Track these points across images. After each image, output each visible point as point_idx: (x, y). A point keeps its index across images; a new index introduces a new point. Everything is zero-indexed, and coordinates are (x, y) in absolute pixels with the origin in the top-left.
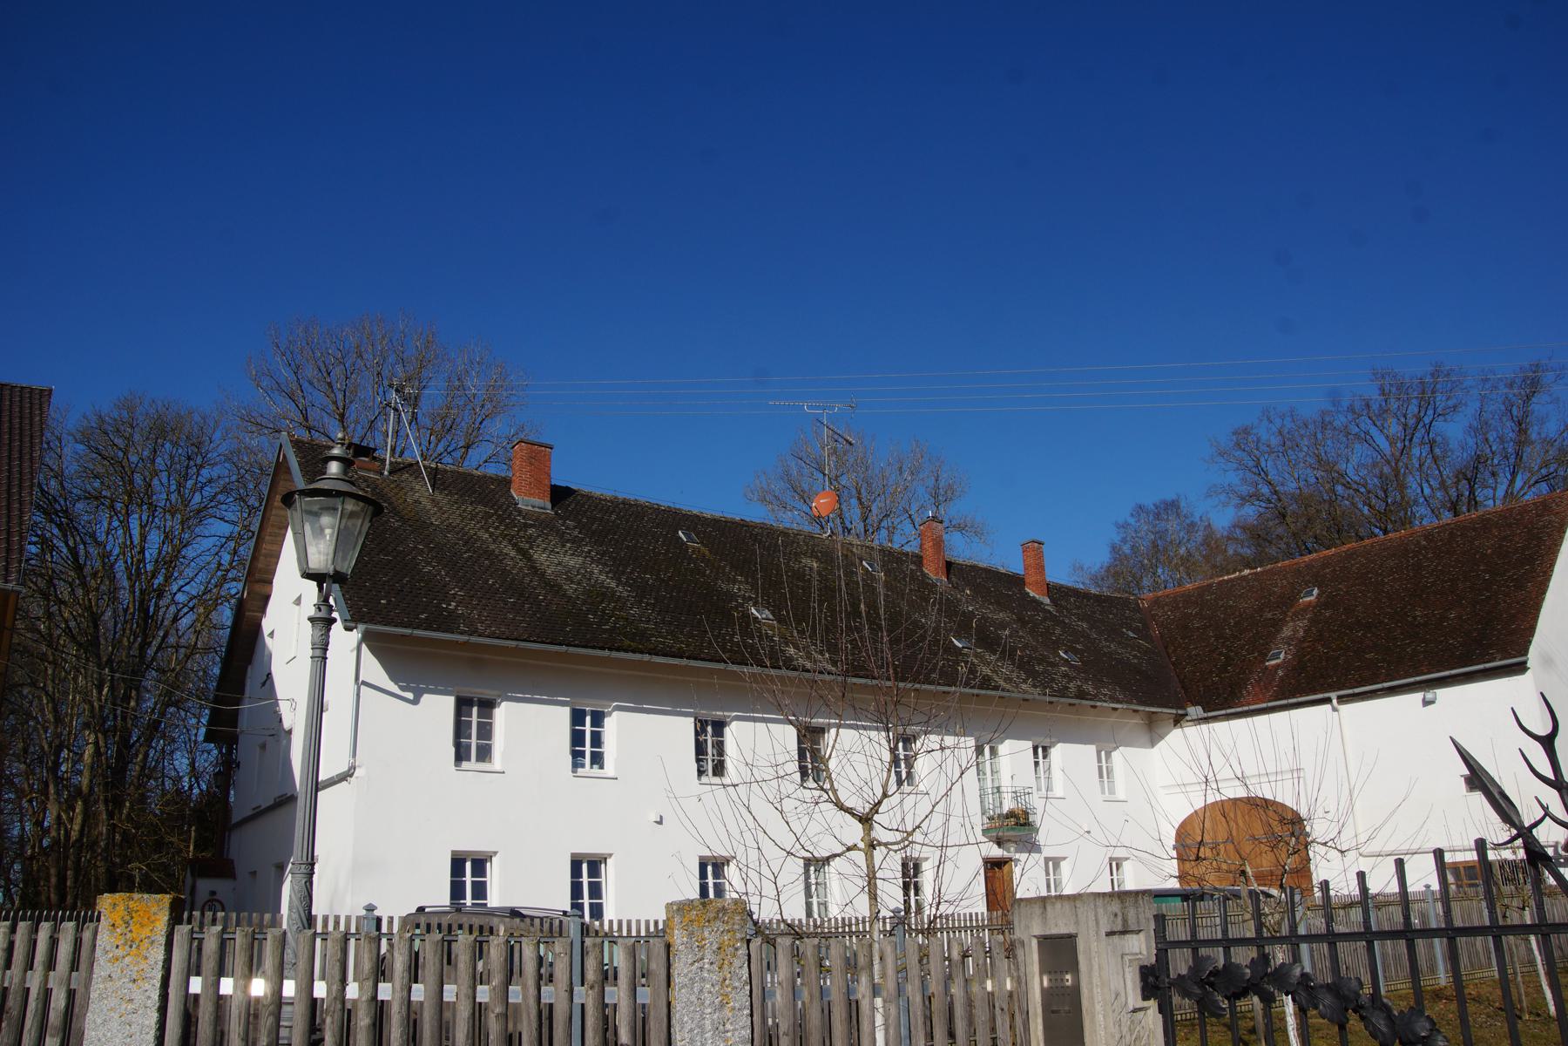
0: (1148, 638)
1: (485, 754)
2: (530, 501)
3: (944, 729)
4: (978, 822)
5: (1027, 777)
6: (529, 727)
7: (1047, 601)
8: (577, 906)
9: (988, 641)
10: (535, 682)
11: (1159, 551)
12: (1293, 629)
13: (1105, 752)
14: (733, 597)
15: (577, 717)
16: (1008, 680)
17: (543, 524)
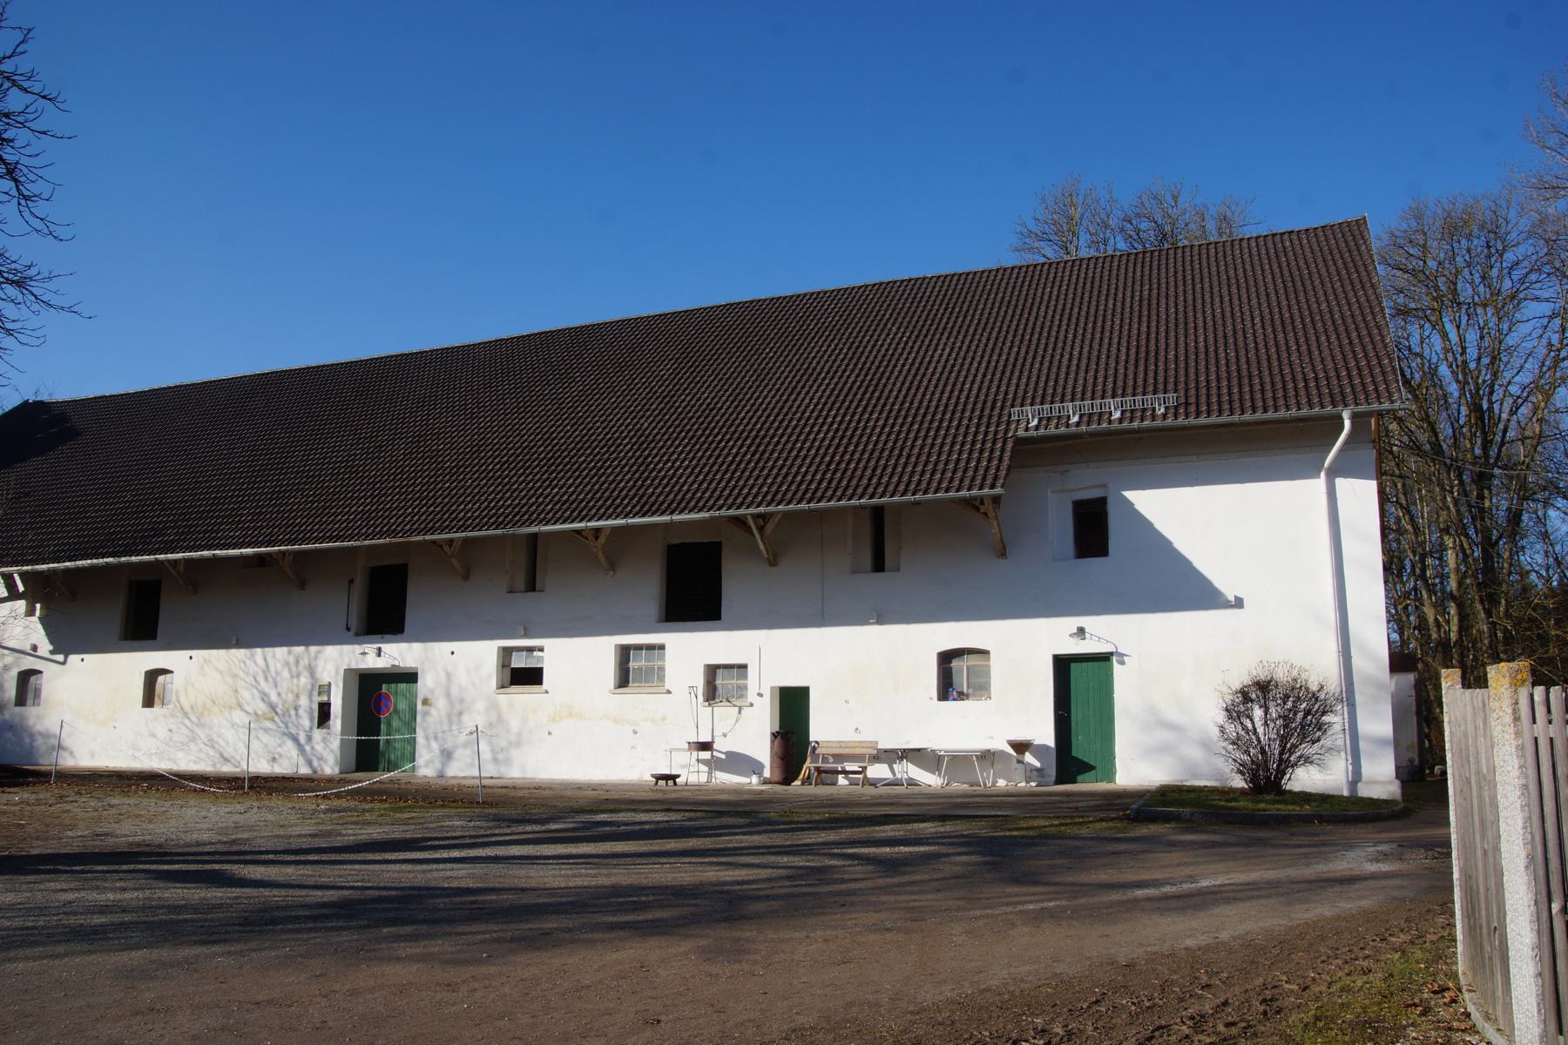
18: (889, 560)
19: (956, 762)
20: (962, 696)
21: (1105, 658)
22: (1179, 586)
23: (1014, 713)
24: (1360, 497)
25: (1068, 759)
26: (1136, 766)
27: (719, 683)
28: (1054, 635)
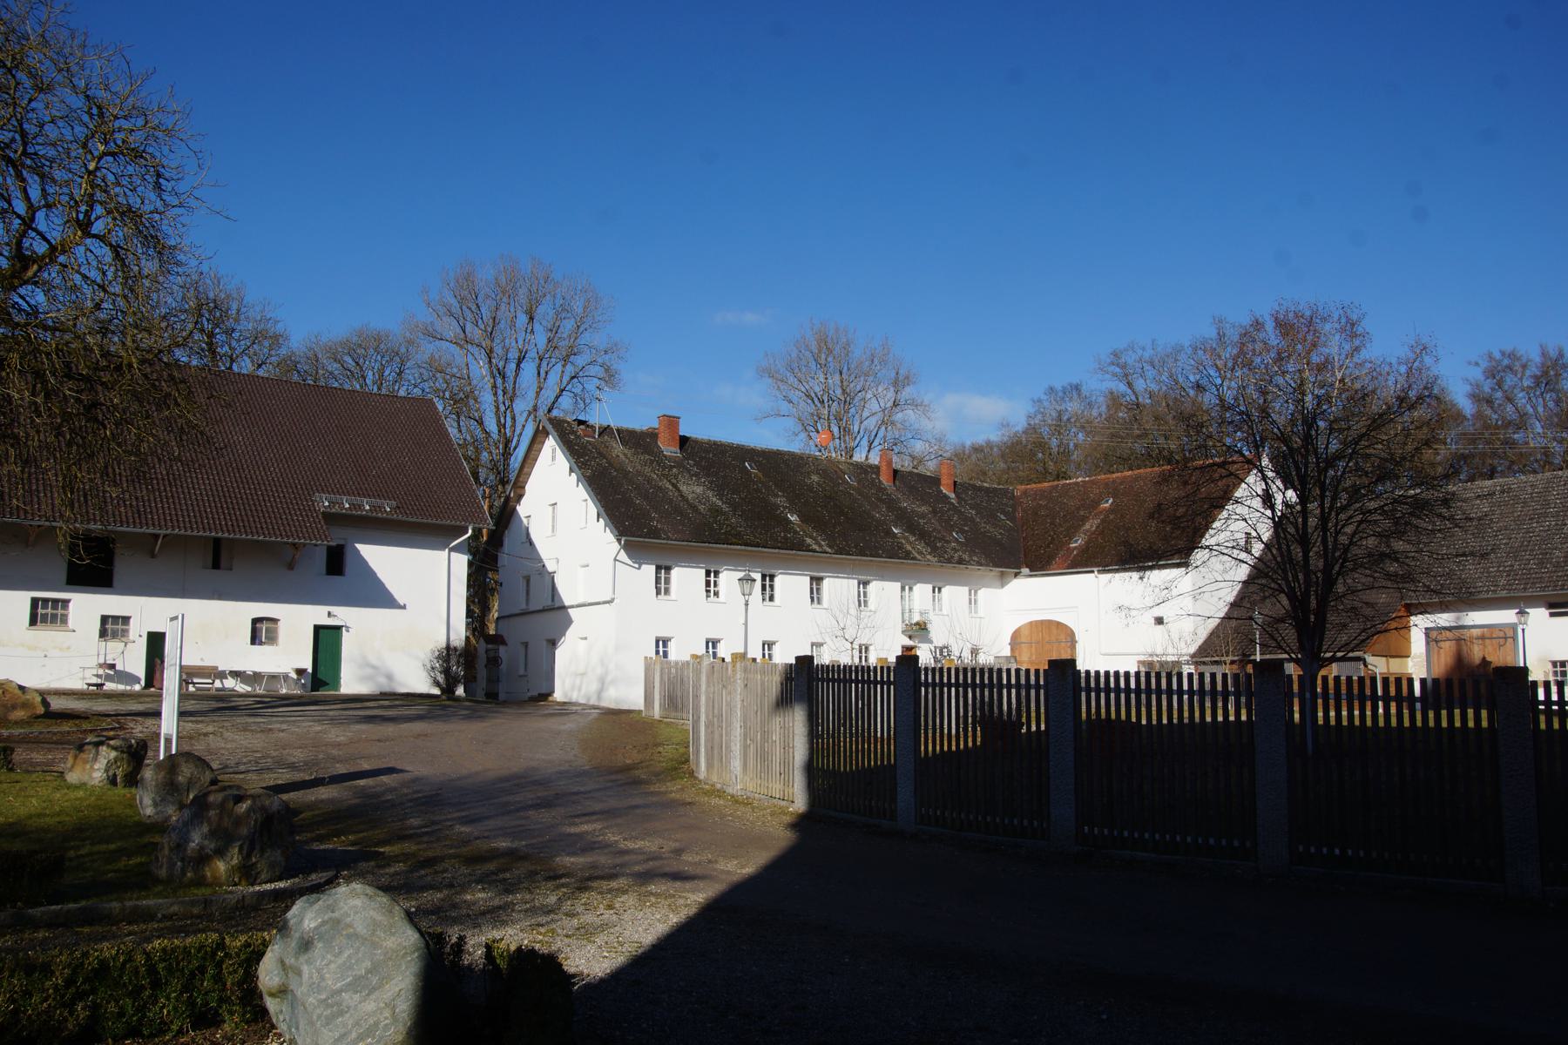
0: (1013, 519)
1: (667, 591)
2: (669, 449)
3: (883, 578)
4: (900, 627)
5: (928, 605)
6: (687, 578)
7: (953, 495)
8: (657, 652)
9: (911, 527)
10: (689, 558)
11: (1060, 425)
12: (1091, 525)
13: (973, 591)
14: (778, 507)
15: (708, 573)
16: (920, 553)
17: (679, 464)
18: (223, 563)
19: (256, 677)
20: (261, 643)
21: (338, 628)
22: (376, 595)
23: (290, 655)
24: (461, 562)
25: (819, 580)
26: (351, 682)
27: (111, 627)
28: (318, 614)
